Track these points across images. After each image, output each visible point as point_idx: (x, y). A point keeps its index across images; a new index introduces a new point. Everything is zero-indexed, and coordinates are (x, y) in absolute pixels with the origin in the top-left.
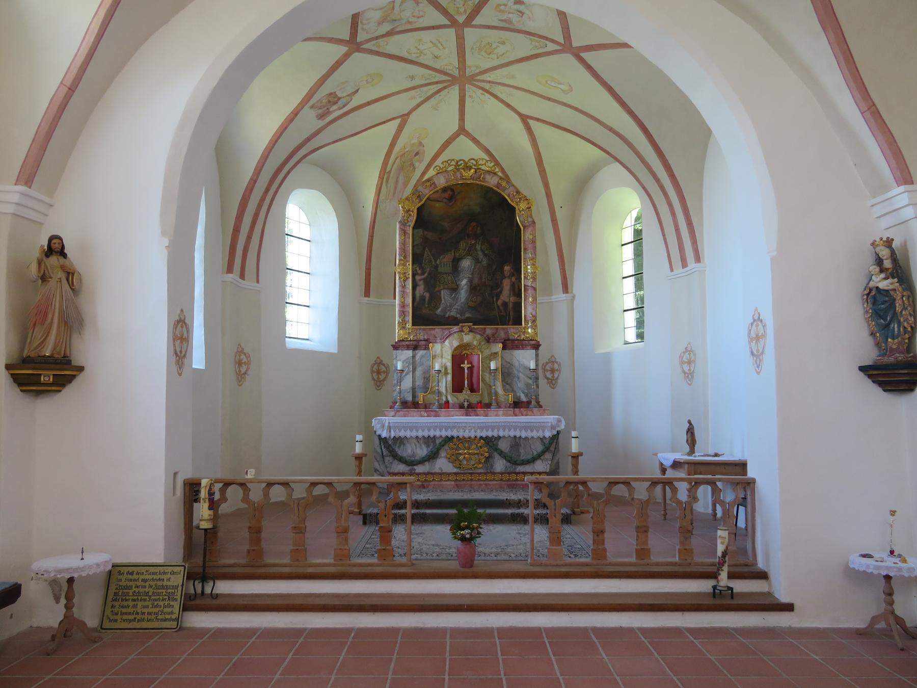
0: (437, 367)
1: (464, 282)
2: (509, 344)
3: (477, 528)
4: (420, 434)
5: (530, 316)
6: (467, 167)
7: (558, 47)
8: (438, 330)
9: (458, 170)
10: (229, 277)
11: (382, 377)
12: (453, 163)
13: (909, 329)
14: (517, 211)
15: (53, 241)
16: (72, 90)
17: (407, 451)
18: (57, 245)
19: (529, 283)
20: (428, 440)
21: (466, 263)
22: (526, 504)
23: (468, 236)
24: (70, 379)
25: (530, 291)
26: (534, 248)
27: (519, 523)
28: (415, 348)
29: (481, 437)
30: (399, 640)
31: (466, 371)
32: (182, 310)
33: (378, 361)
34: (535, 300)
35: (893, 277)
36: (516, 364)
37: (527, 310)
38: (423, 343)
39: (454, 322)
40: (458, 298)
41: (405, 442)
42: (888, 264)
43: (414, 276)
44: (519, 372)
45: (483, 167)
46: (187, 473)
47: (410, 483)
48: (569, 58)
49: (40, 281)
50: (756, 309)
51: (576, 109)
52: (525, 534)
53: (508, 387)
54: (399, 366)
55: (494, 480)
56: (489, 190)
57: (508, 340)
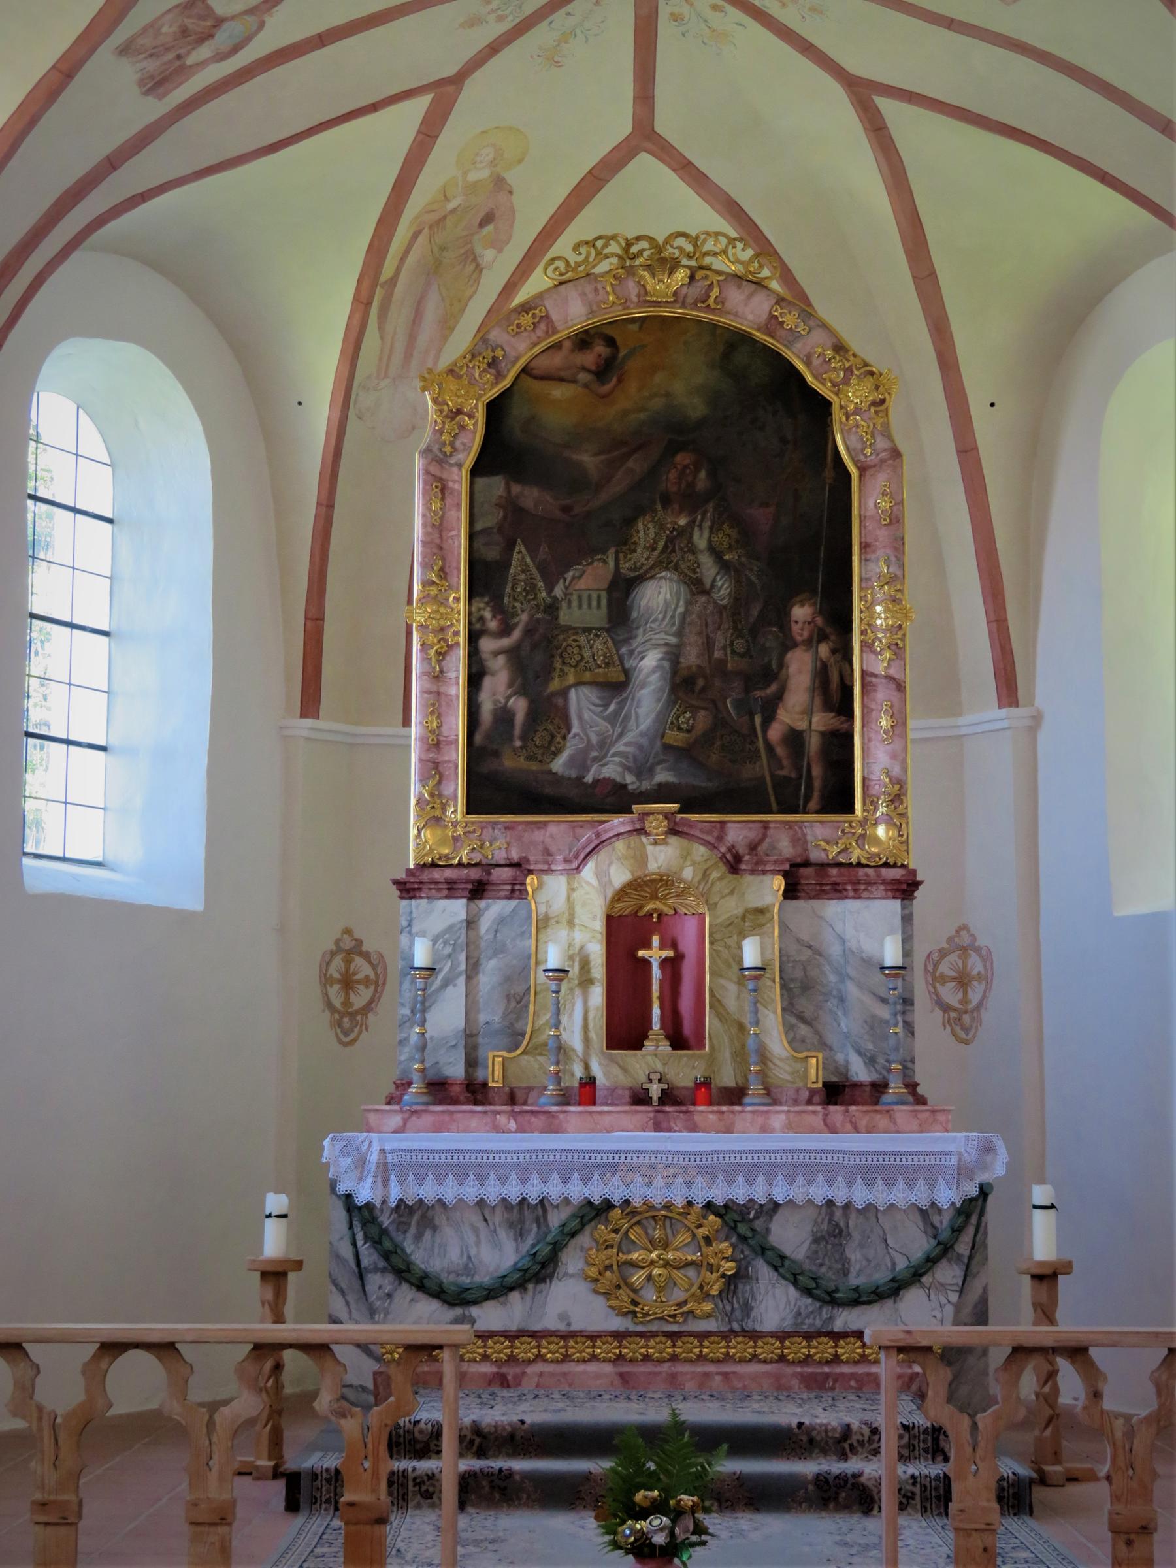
0: (554, 957)
2: (804, 880)
3: (693, 1509)
4: (493, 1191)
5: (880, 780)
6: (664, 263)
8: (556, 830)
9: (631, 271)
11: (360, 998)
12: (614, 248)
14: (837, 415)
17: (441, 1254)
19: (879, 666)
20: (523, 1214)
21: (658, 596)
22: (870, 1442)
23: (666, 501)
25: (883, 694)
26: (898, 546)
27: (846, 1507)
28: (478, 891)
29: (709, 1206)
31: (656, 972)
33: (348, 944)
34: (899, 723)
37: (870, 761)
38: (506, 874)
39: (616, 799)
40: (622, 722)
41: (440, 1219)
43: (473, 637)
44: (843, 977)
45: (718, 263)
47: (455, 1346)
52: (866, 1547)
53: (803, 1030)
54: (421, 955)
55: (754, 1358)
56: (737, 341)
57: (806, 864)
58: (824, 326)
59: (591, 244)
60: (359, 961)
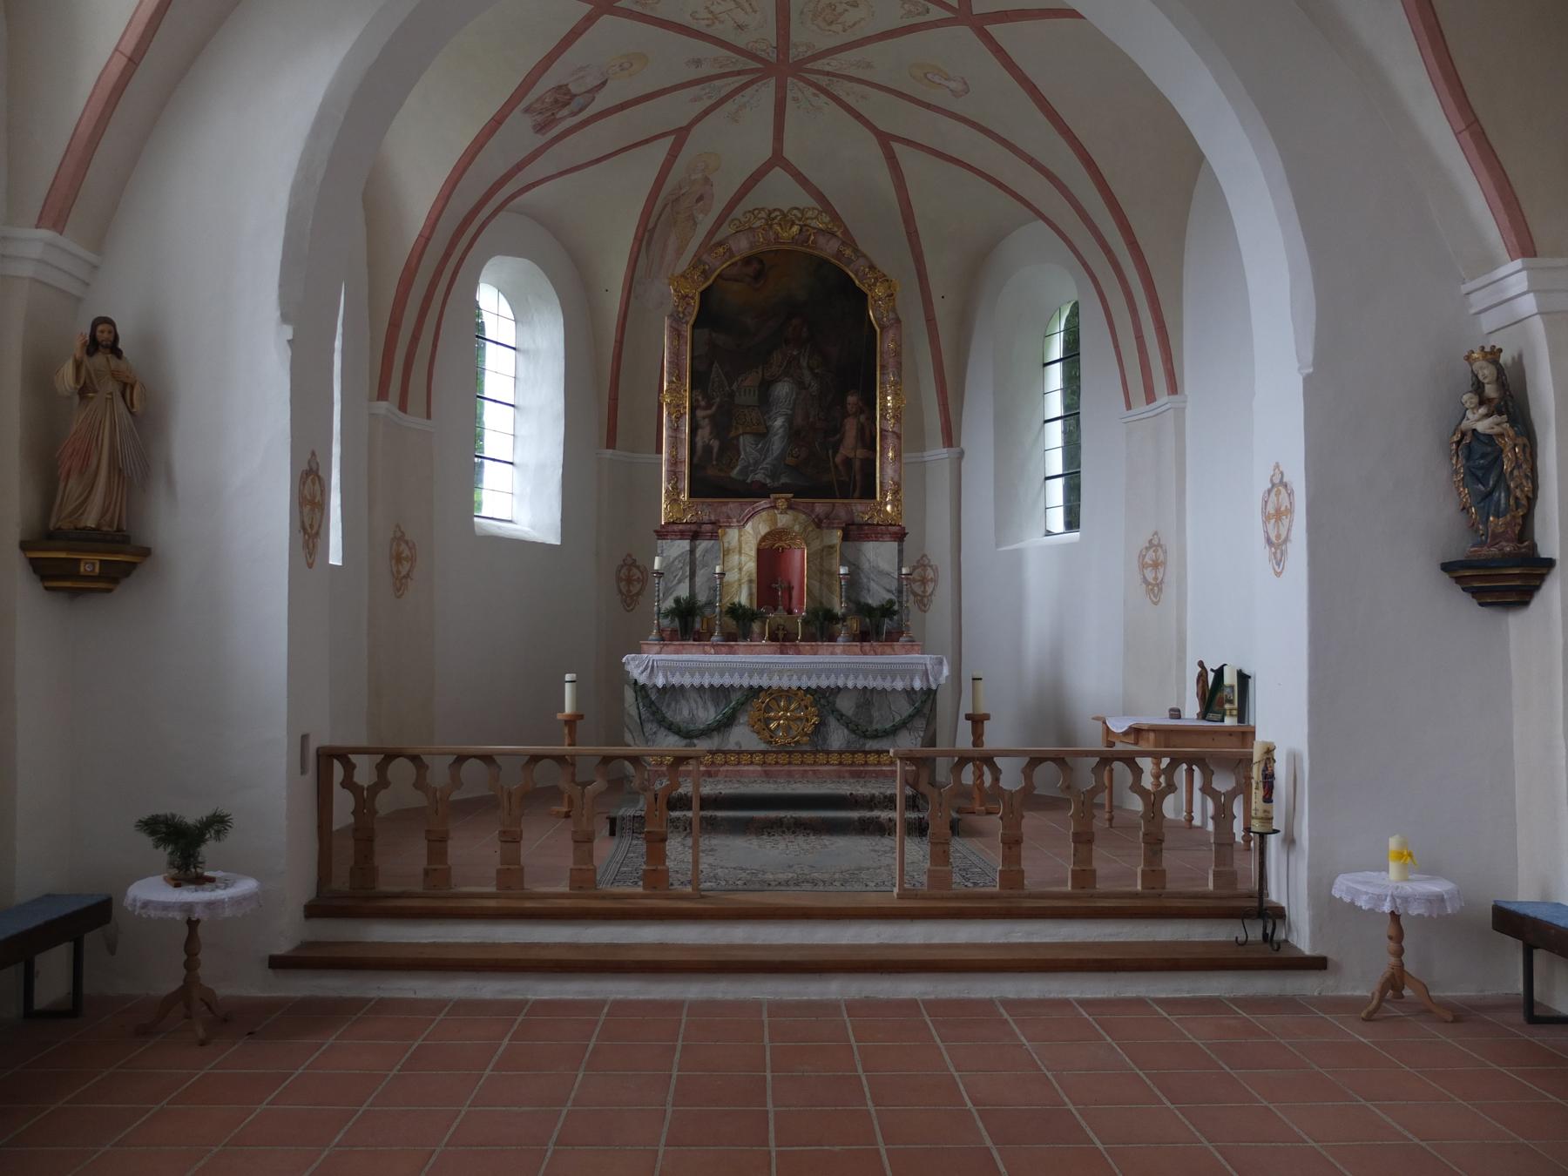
1: (779, 422)
2: (855, 532)
7: (947, 14)
8: (732, 506)
9: (771, 226)
10: (383, 407)
11: (635, 588)
12: (763, 214)
13: (1524, 502)
15: (100, 328)
16: (134, 61)
18: (106, 335)
20: (719, 693)
21: (783, 389)
22: (889, 802)
24: (127, 570)
25: (890, 441)
27: (872, 833)
28: (695, 536)
30: (684, 1019)
32: (313, 454)
33: (629, 561)
35: (1500, 414)
36: (866, 566)
37: (885, 471)
38: (708, 527)
39: (761, 491)
40: (767, 446)
42: (1491, 391)
43: (693, 409)
45: (814, 223)
46: (323, 737)
48: (965, 32)
49: (77, 398)
50: (1277, 466)
51: (973, 125)
56: (823, 262)
58: (864, 256)
59: (752, 212)
60: (635, 570)
